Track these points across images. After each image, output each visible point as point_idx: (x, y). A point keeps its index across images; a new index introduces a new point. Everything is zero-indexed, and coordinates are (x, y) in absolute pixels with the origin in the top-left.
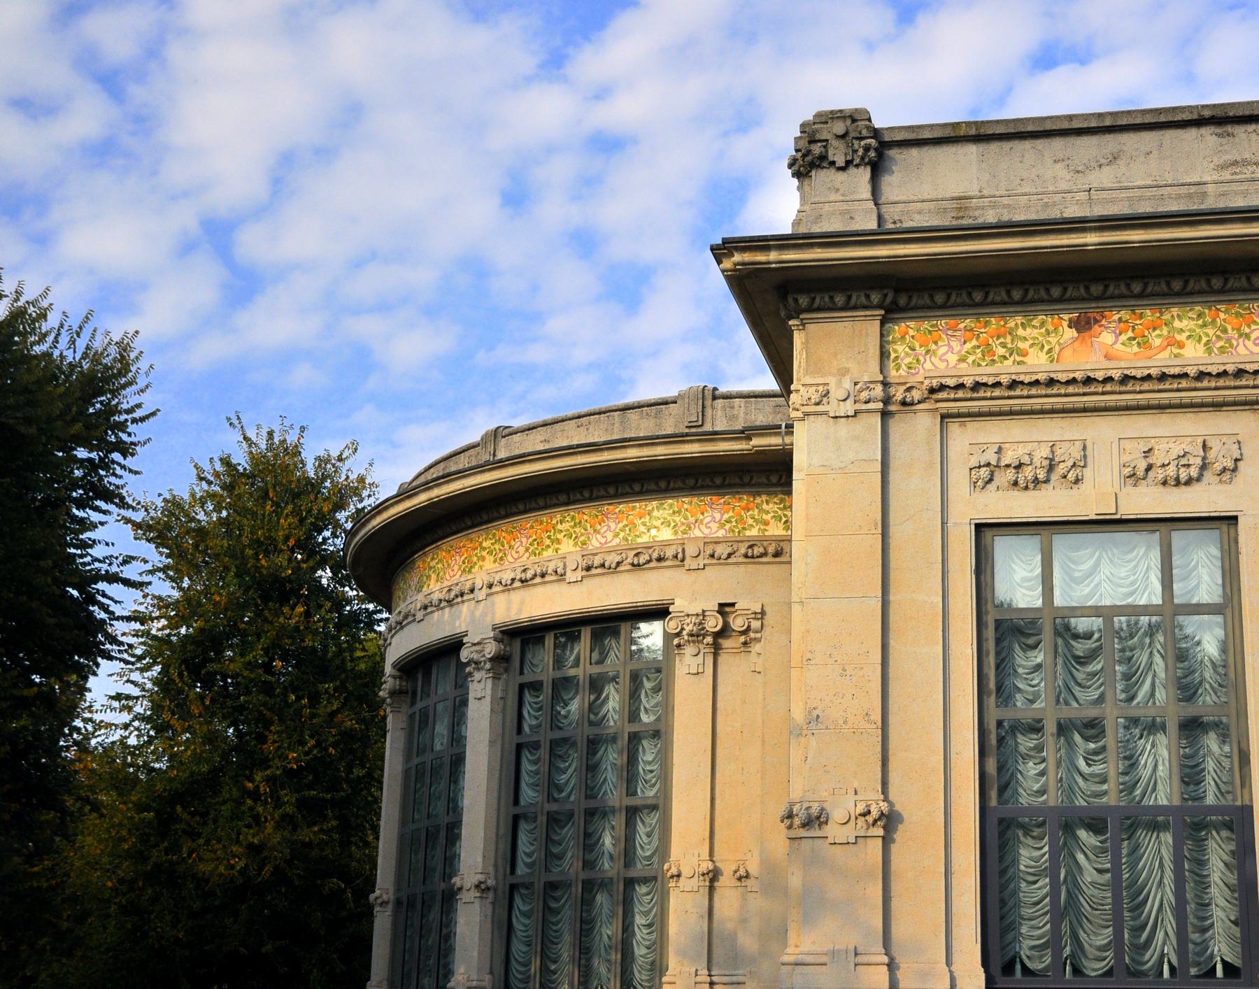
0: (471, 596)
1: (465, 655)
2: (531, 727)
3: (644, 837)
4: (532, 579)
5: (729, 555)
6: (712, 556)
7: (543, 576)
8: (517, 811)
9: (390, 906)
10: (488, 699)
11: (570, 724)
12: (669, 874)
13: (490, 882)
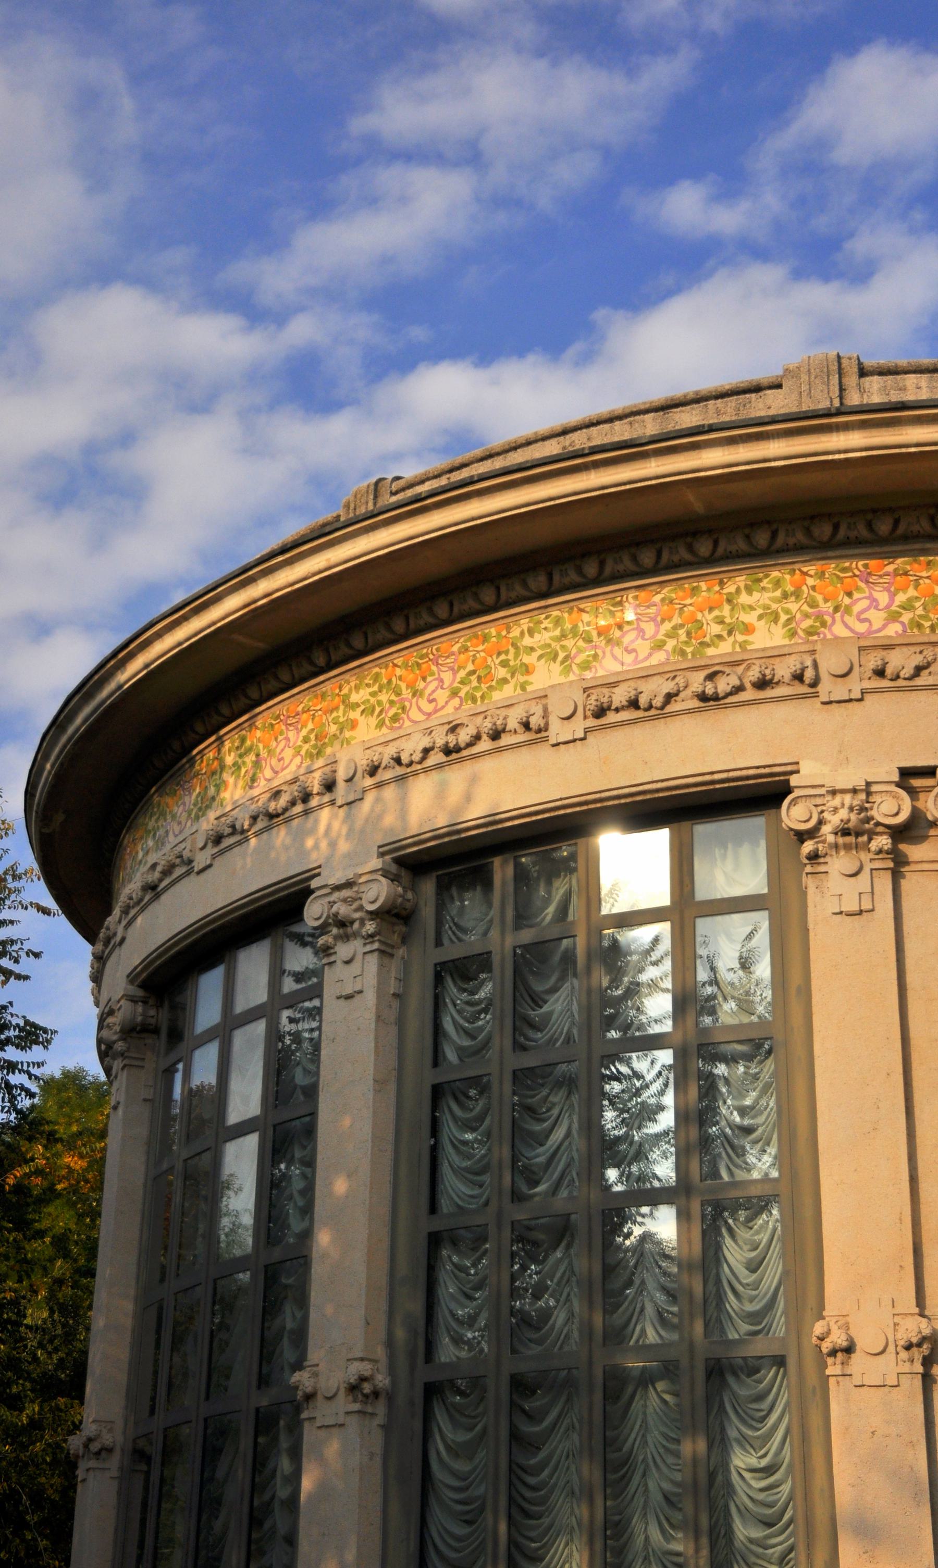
0: (327, 798)
1: (314, 912)
2: (462, 1052)
3: (742, 1272)
4: (470, 745)
5: (919, 670)
6: (880, 673)
7: (496, 735)
8: (437, 1225)
9: (114, 1462)
10: (370, 997)
11: (552, 1041)
12: (826, 1346)
13: (382, 1380)
